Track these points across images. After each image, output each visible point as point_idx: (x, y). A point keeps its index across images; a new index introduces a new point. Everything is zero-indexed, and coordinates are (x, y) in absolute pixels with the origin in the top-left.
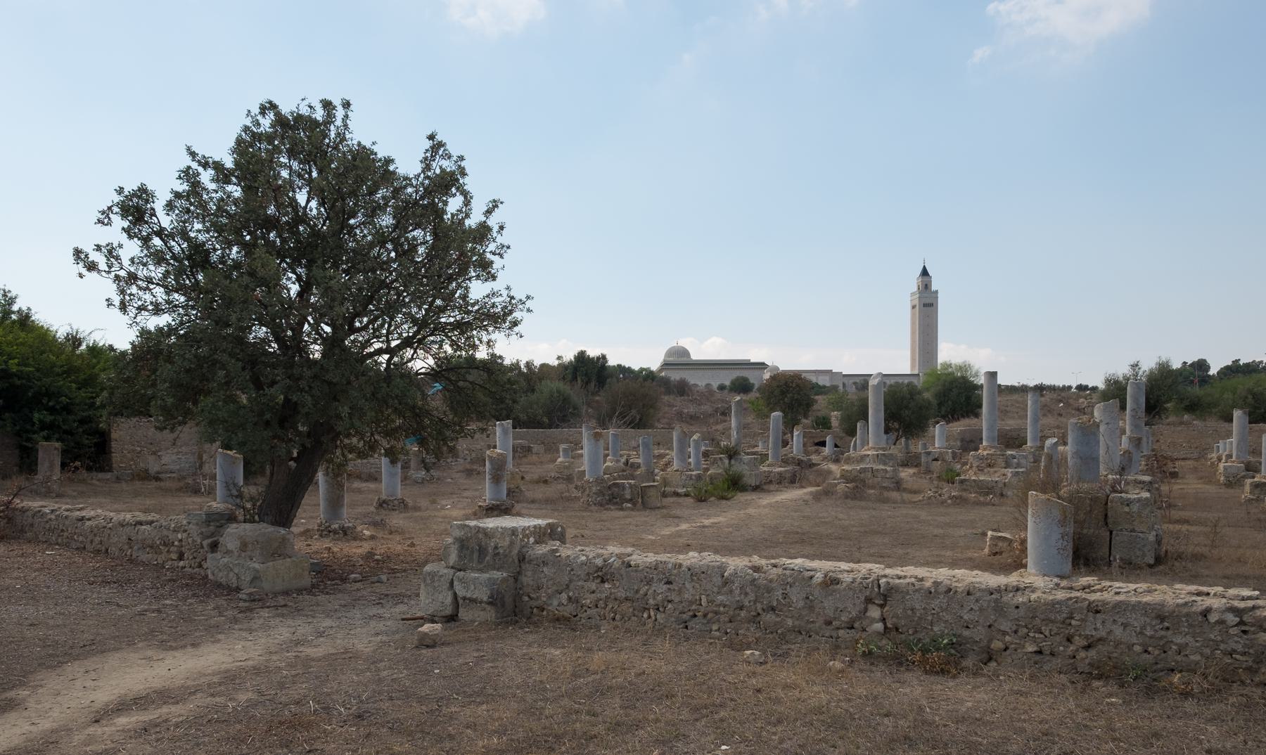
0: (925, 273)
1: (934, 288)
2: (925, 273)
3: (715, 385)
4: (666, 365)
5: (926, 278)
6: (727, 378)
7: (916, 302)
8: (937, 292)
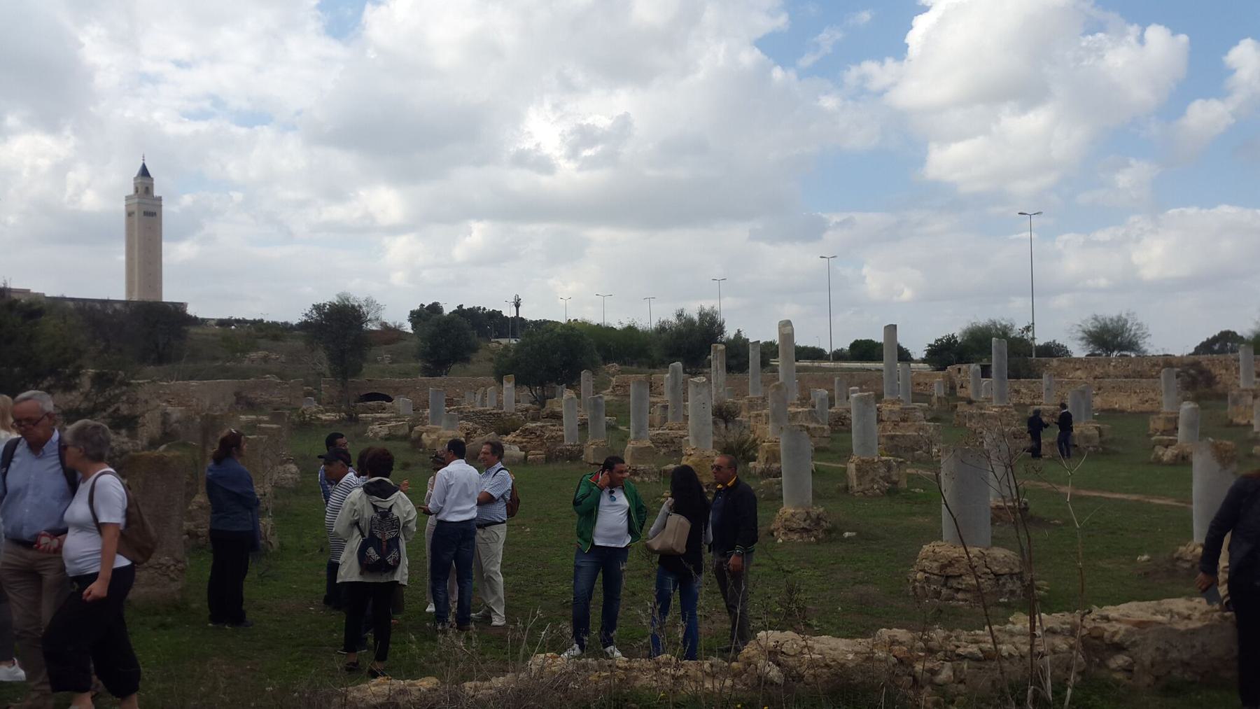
0: (144, 172)
1: (156, 193)
2: (144, 172)
5: (146, 180)
7: (134, 208)
8: (160, 199)
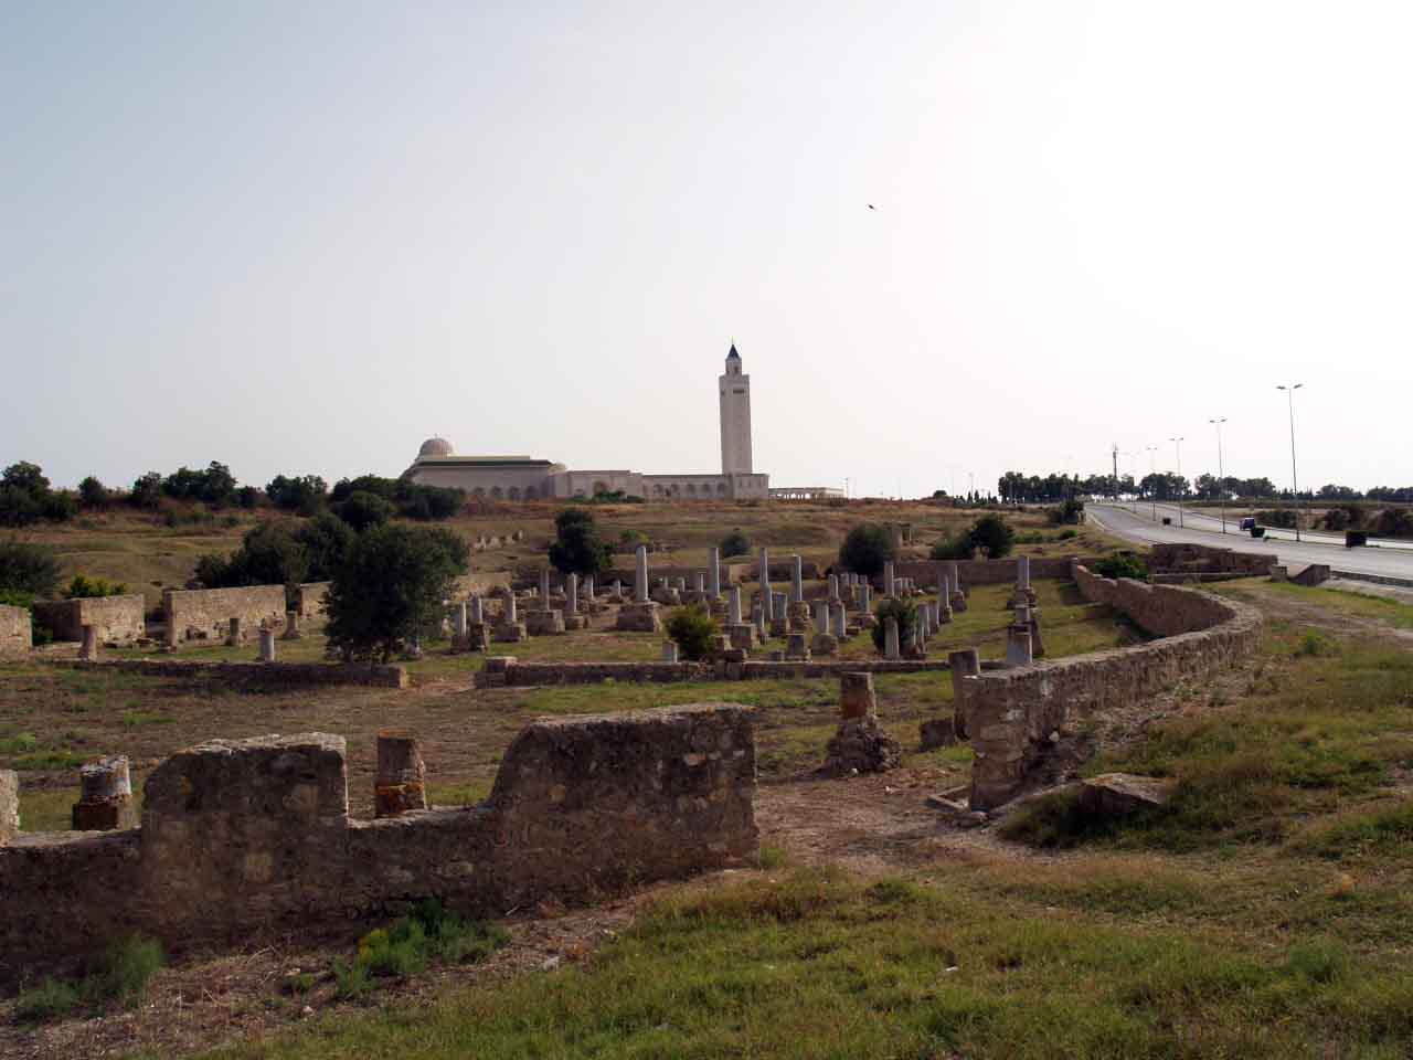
0: (733, 353)
2: (733, 353)
3: (505, 487)
4: (422, 465)
6: (520, 481)
8: (747, 377)
